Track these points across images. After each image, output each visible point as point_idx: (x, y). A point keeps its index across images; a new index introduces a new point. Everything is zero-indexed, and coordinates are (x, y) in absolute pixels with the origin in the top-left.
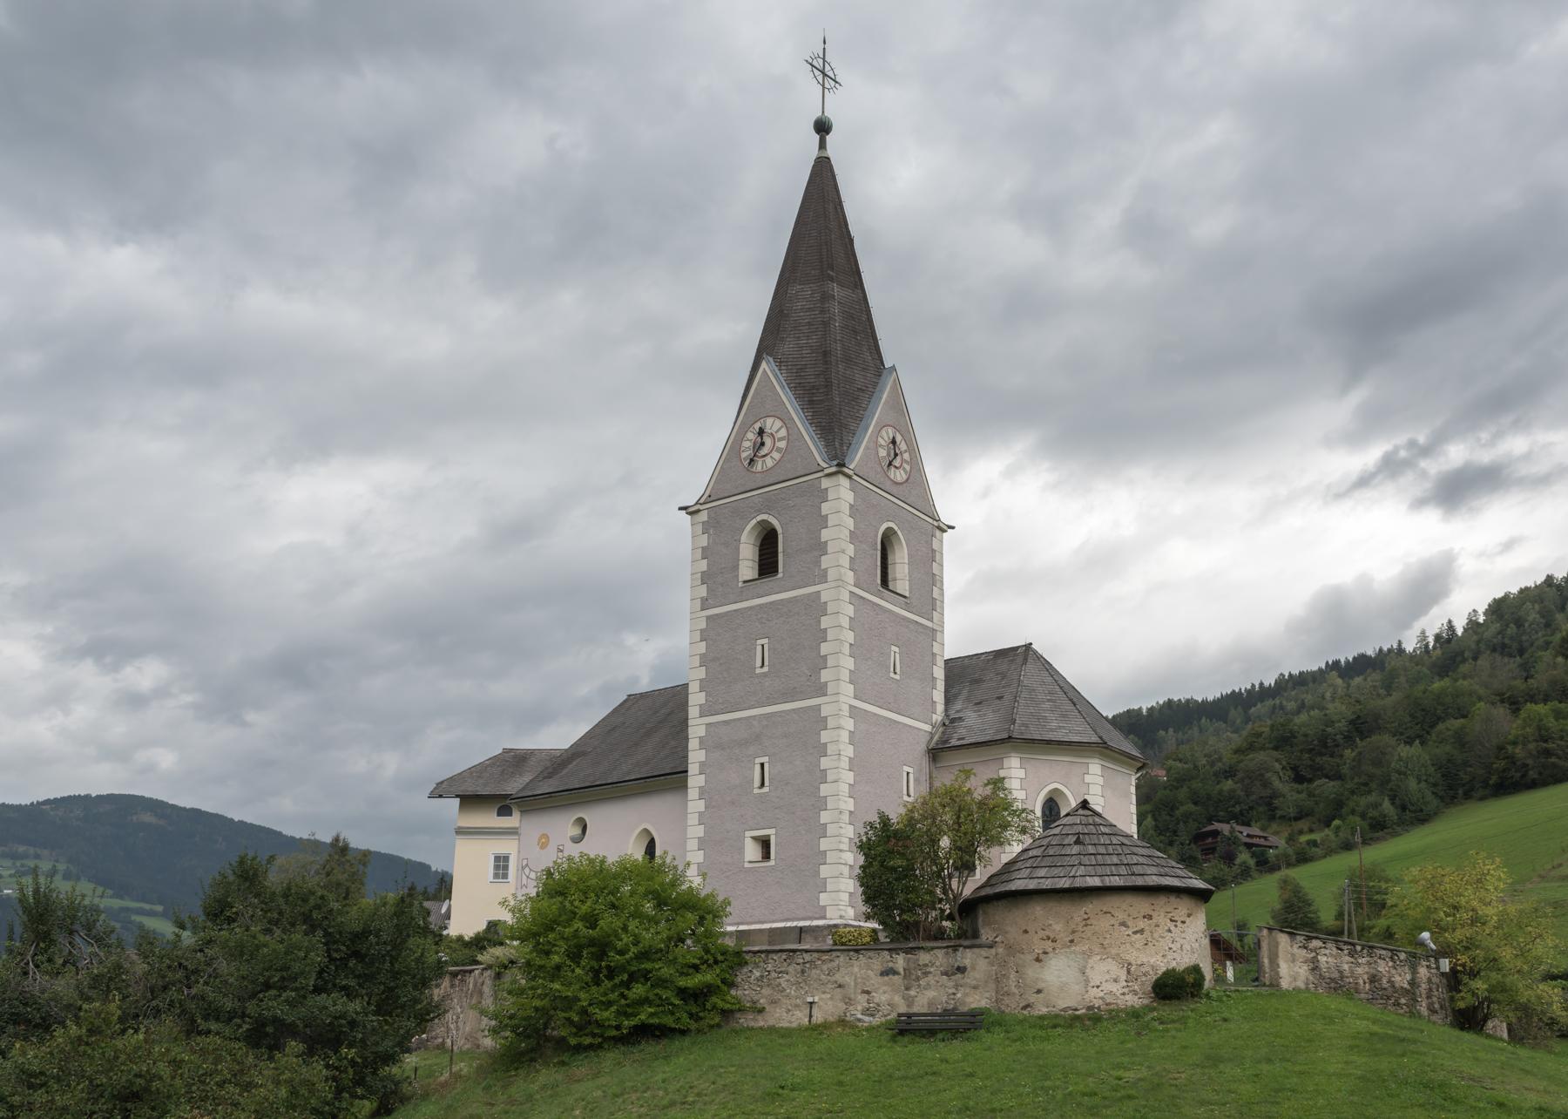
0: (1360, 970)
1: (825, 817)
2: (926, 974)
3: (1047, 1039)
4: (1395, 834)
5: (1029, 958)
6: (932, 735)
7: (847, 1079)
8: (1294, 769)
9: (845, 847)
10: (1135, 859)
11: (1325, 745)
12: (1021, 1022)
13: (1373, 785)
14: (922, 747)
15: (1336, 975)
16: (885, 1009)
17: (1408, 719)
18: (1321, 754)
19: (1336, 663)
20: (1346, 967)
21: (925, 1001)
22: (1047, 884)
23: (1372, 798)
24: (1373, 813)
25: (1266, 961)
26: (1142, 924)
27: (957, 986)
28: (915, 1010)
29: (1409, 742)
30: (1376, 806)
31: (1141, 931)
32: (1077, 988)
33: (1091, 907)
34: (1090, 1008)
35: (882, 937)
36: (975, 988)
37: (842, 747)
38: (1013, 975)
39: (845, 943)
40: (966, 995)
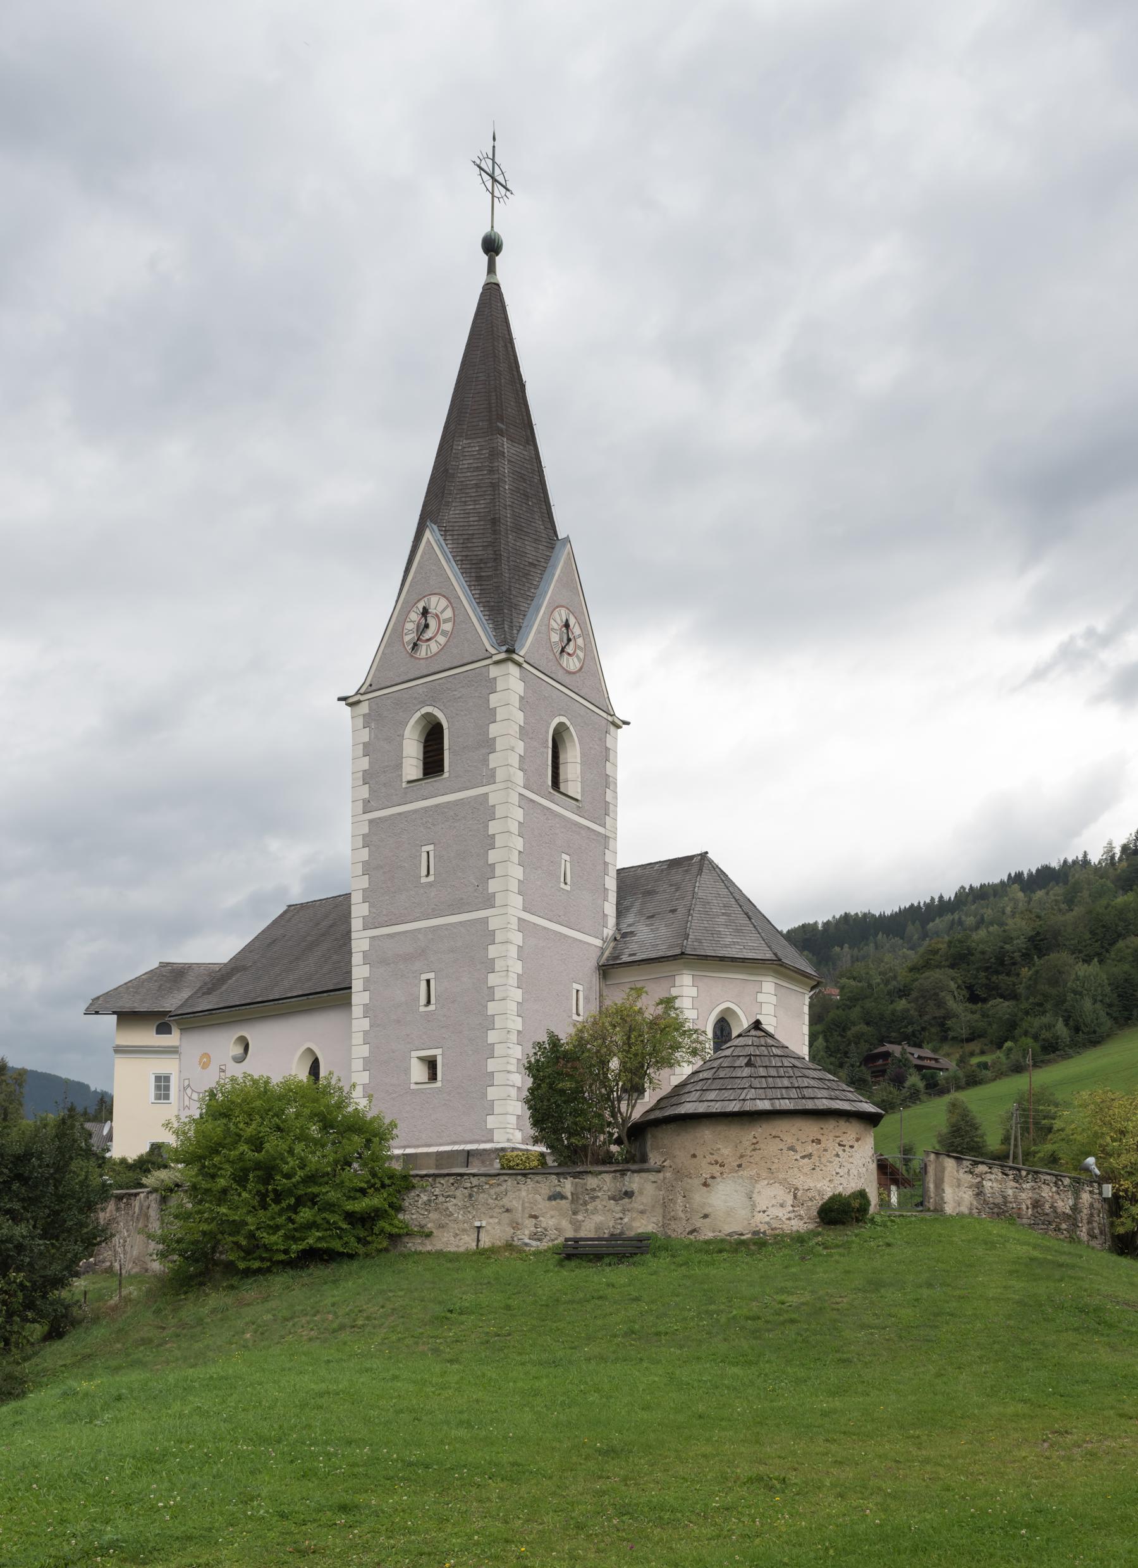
0: (1023, 1195)
1: (492, 1037)
2: (594, 1198)
3: (708, 1264)
4: (1067, 1057)
5: (697, 1182)
6: (603, 950)
7: (514, 1303)
8: (970, 988)
9: (513, 1068)
10: (806, 1082)
11: (1002, 963)
12: (687, 1247)
13: (1048, 1006)
14: (592, 963)
15: (1000, 1200)
16: (553, 1233)
17: (1088, 936)
18: (997, 973)
19: (1019, 875)
20: (1010, 1192)
21: (592, 1226)
22: (717, 1108)
23: (1045, 1020)
24: (1045, 1035)
25: (932, 1186)
26: (810, 1148)
27: (624, 1211)
28: (582, 1234)
29: (1087, 960)
30: (1049, 1027)
31: (810, 1156)
32: (743, 1213)
33: (761, 1131)
34: (756, 1233)
35: (550, 1160)
36: (642, 1212)
37: (510, 962)
38: (680, 1200)
39: (513, 1167)
40: (633, 1219)
